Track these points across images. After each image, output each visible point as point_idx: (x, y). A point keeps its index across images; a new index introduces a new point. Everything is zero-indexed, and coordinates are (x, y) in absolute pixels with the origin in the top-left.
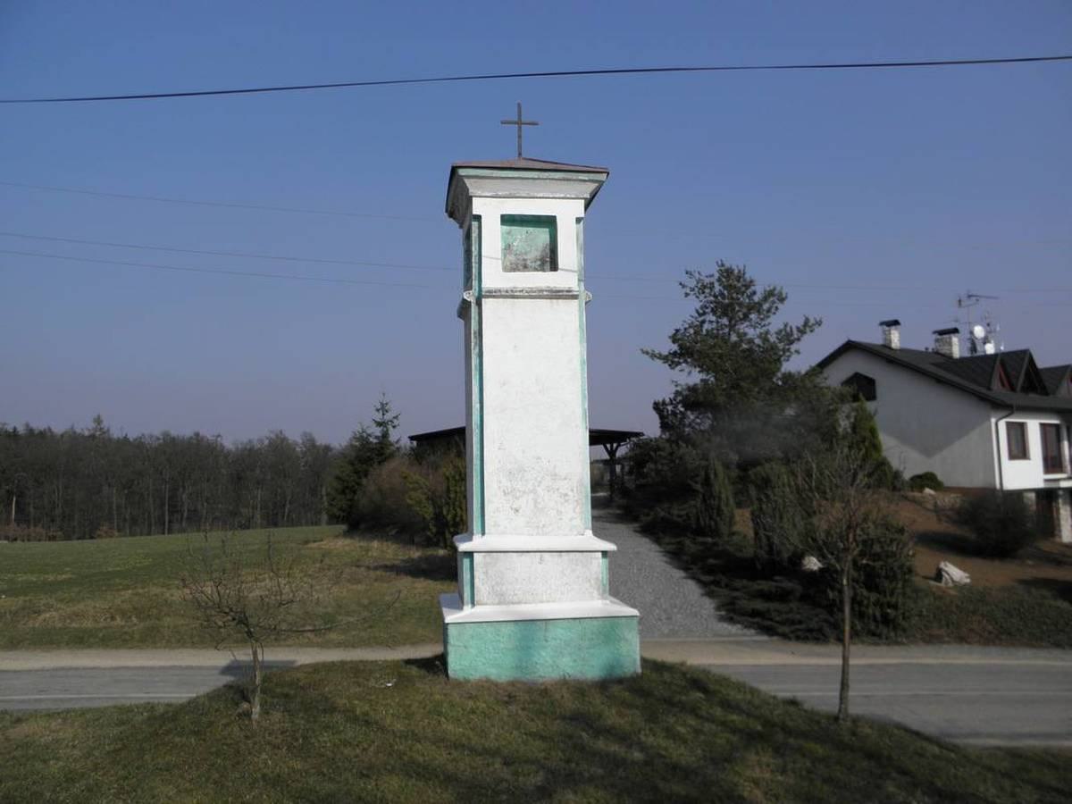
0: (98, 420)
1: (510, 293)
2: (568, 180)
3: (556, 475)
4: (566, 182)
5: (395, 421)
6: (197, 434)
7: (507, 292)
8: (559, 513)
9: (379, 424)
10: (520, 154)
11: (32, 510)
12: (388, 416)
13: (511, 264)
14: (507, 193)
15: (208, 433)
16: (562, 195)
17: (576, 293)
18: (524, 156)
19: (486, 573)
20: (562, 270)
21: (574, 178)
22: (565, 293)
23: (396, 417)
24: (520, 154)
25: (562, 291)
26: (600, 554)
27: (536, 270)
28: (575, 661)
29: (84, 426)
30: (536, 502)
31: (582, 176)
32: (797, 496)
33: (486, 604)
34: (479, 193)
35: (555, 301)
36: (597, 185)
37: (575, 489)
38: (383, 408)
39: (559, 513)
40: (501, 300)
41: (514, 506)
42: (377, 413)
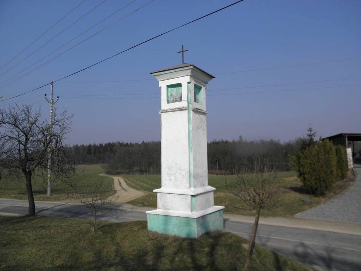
0: (241, 137)
1: (167, 111)
2: (182, 70)
3: (181, 169)
4: (182, 71)
5: (315, 134)
6: (272, 140)
7: (167, 110)
8: (182, 181)
9: (309, 136)
10: (183, 62)
11: (222, 165)
12: (312, 133)
13: (172, 100)
14: (167, 78)
15: (275, 139)
16: (182, 76)
17: (185, 108)
18: (184, 63)
19: (160, 199)
20: (183, 101)
21: (183, 69)
22: (182, 109)
23: (315, 133)
24: (183, 62)
25: (181, 108)
26: (190, 196)
27: (179, 101)
28: (178, 230)
29: (237, 139)
30: (176, 178)
31: (185, 68)
32: (38, 193)
33: (160, 209)
34: (160, 80)
35: (181, 111)
36: (191, 70)
37: (186, 174)
38: (310, 130)
39: (182, 181)
40: (166, 113)
41: (170, 179)
42: (308, 132)
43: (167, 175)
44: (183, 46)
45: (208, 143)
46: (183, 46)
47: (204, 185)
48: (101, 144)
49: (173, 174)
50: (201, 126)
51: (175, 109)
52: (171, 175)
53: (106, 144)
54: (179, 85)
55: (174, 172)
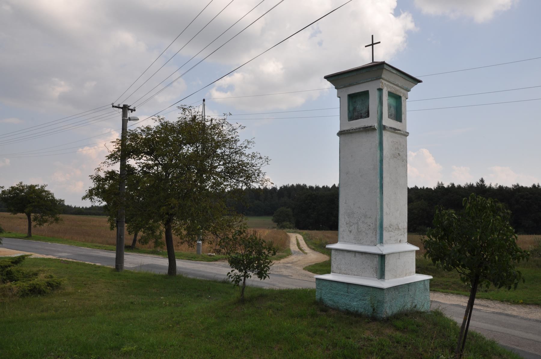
27: (365, 117)
30: (358, 229)
43: (347, 224)
47: (400, 241)
51: (360, 128)
53: (281, 188)
54: (366, 94)
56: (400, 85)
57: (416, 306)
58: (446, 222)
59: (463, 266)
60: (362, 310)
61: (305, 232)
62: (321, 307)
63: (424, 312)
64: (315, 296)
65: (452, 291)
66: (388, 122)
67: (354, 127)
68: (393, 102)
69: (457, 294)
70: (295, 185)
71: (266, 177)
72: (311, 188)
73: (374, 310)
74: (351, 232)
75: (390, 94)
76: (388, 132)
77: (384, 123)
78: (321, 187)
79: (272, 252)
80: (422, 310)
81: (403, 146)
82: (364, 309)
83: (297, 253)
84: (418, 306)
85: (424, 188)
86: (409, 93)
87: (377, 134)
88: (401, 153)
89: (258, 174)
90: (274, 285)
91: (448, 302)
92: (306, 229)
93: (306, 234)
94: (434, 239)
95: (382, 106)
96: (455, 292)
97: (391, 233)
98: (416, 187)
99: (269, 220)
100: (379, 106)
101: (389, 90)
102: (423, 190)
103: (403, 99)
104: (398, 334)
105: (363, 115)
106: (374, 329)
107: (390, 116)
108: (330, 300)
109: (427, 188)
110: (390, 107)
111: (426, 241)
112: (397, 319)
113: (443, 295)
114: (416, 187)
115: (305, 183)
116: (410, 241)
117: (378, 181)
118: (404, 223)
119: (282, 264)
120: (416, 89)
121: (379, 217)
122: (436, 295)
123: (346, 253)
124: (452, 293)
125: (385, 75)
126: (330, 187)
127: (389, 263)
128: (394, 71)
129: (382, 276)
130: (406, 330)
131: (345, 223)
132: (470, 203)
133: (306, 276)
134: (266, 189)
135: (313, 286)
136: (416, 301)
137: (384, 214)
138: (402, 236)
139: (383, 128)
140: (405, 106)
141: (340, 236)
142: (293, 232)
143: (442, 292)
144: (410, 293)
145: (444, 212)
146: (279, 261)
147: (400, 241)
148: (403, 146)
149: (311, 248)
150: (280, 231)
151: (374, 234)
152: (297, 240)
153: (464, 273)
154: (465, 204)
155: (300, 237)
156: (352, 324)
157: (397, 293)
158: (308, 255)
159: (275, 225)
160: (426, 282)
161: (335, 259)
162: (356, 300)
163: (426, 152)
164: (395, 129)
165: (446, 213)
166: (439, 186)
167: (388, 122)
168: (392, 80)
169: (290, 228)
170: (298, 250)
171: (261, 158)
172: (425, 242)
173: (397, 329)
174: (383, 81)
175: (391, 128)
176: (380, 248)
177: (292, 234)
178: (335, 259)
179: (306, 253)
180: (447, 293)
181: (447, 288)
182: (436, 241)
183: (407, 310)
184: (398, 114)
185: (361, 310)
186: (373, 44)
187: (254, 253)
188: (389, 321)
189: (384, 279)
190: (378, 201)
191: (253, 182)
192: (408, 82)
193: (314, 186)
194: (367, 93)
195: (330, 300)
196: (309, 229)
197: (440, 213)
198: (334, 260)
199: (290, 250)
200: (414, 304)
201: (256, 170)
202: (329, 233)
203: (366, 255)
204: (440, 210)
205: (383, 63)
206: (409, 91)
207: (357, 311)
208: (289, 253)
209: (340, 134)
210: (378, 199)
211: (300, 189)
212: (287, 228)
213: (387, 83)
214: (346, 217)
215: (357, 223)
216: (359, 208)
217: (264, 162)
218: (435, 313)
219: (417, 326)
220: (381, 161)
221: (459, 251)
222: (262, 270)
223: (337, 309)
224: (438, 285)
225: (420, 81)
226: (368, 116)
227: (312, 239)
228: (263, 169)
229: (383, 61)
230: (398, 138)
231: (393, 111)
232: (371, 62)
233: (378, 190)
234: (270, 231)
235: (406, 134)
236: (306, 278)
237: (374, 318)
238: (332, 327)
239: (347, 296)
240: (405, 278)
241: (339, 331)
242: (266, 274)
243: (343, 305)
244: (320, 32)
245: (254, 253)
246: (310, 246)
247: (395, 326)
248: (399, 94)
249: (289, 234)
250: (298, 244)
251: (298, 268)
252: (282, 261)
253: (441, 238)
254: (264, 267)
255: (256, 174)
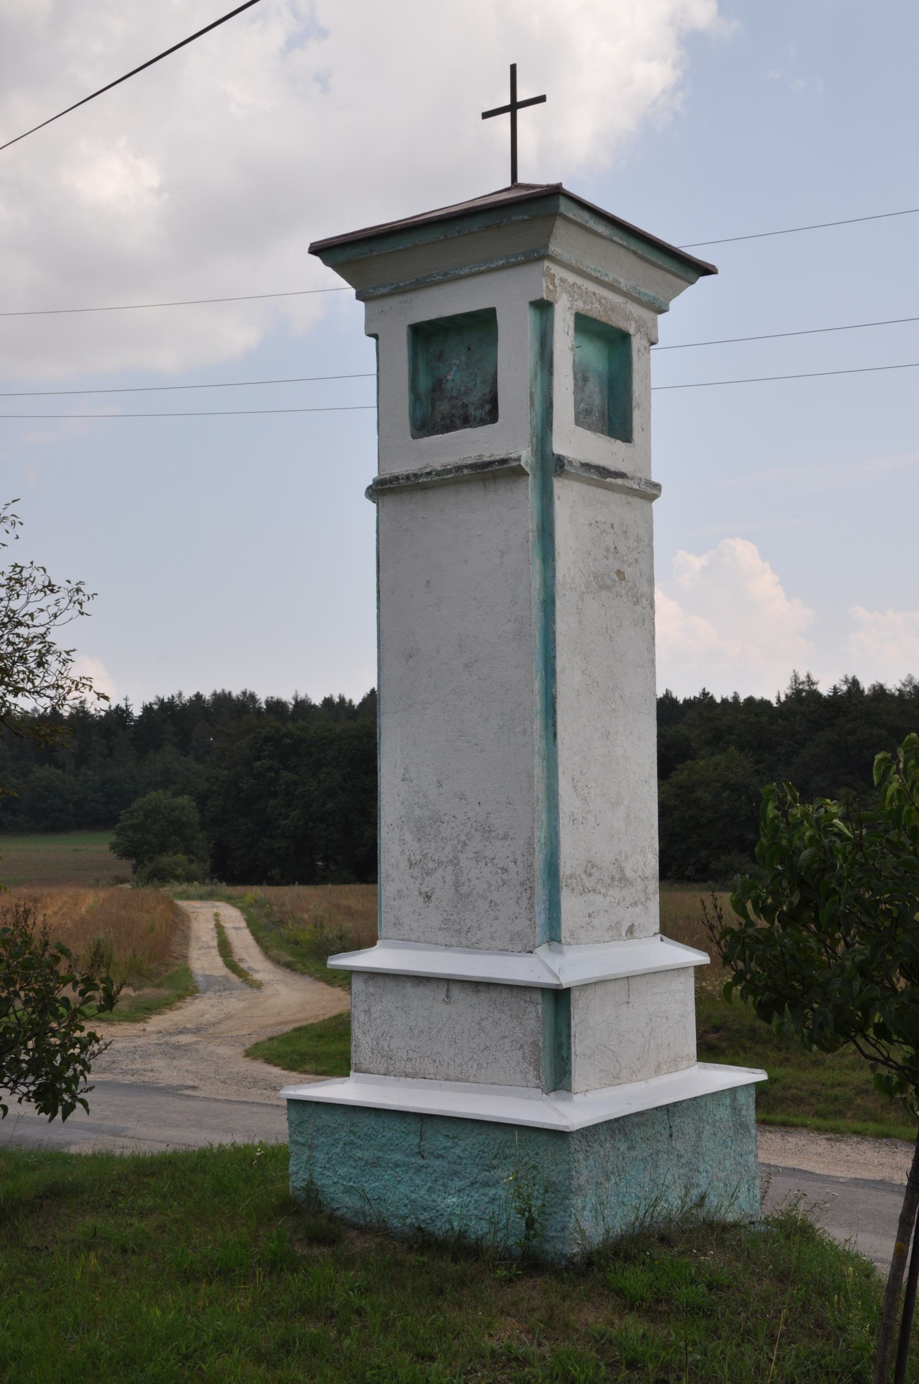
27: (483, 422)
30: (457, 884)
41: (424, 889)
43: (412, 865)
44: (513, 68)
45: (574, 361)
46: (513, 68)
47: (631, 931)
48: (123, 706)
49: (440, 863)
50: (619, 572)
51: (459, 468)
52: (431, 865)
53: (147, 709)
54: (485, 321)
55: (448, 849)
56: (624, 284)
57: (703, 1198)
58: (806, 853)
59: (882, 1031)
60: (484, 1227)
61: (255, 892)
62: (315, 1223)
63: (735, 1225)
64: (286, 1178)
65: (859, 1126)
66: (573, 441)
67: (437, 464)
68: (595, 356)
69: (879, 1136)
70: (207, 695)
71: (75, 672)
72: (276, 706)
73: (530, 1223)
74: (428, 897)
75: (585, 325)
76: (576, 486)
77: (560, 446)
78: (317, 701)
79: (99, 994)
80: (731, 1218)
81: (638, 539)
82: (491, 1222)
83: (223, 986)
84: (713, 1200)
85: (736, 698)
86: (660, 317)
87: (527, 494)
88: (628, 571)
89: (42, 655)
90: (116, 1133)
91: (842, 1172)
92: (258, 882)
93: (258, 904)
94: (762, 923)
95: (551, 373)
96: (872, 1126)
97: (592, 896)
98: (705, 694)
99: (97, 847)
100: (538, 373)
101: (580, 306)
102: (731, 706)
103: (637, 343)
104: (634, 1326)
105: (471, 410)
106: (531, 1311)
107: (582, 418)
108: (348, 1191)
109: (750, 700)
110: (585, 379)
111: (728, 931)
112: (627, 1258)
113: (821, 1144)
114: (705, 694)
115: (250, 689)
116: (672, 928)
117: (537, 685)
118: (645, 855)
119: (154, 1039)
120: (690, 302)
121: (541, 835)
122: (795, 1140)
123: (409, 989)
124: (857, 1133)
125: (564, 242)
126: (357, 701)
127: (588, 1025)
128: (602, 228)
129: (559, 1078)
130: (663, 1307)
131: (404, 864)
132: (905, 772)
133: (255, 1083)
134: (81, 714)
135: (274, 1129)
136: (702, 1180)
137: (563, 821)
138: (638, 909)
139: (553, 466)
140: (647, 375)
141: (386, 918)
142: (201, 898)
143: (819, 1130)
144: (678, 1145)
145: (797, 811)
146: (140, 1026)
147: (631, 931)
148: (638, 539)
149: (277, 962)
150: (148, 891)
151: (524, 902)
152: (220, 928)
153: (887, 1061)
154: (885, 776)
155: (232, 917)
156: (441, 1291)
157: (623, 1147)
158: (267, 991)
159: (126, 866)
160: (742, 1098)
161: (368, 1012)
162: (457, 1183)
163: (745, 552)
164: (603, 472)
165: (805, 815)
166: (798, 692)
167: (573, 441)
168: (590, 265)
169: (190, 878)
170: (225, 971)
171: (50, 588)
172: (723, 936)
173: (630, 1304)
174: (555, 270)
175: (587, 466)
176: (549, 961)
177: (197, 904)
178: (368, 1012)
179: (257, 986)
180: (836, 1133)
181: (839, 1114)
182: (770, 932)
183: (669, 1220)
184: (615, 409)
185: (478, 1228)
186: (514, 107)
187: (18, 1004)
188: (596, 1268)
189: (569, 1090)
190: (538, 771)
191: (17, 691)
192: (657, 274)
193: (288, 697)
194: (487, 313)
195: (348, 1191)
196: (271, 882)
197: (785, 814)
198: (362, 1018)
199: (187, 972)
200: (695, 1193)
201: (29, 642)
202: (349, 895)
203: (494, 994)
204: (782, 805)
205: (555, 192)
206: (661, 311)
207: (462, 1234)
208: (185, 987)
209: (380, 490)
210: (537, 760)
211: (230, 711)
212: (177, 878)
213: (571, 278)
214: (408, 837)
215: (455, 862)
216: (462, 797)
217: (64, 604)
218: (780, 1224)
219: (710, 1287)
220: (549, 604)
221: (862, 970)
222: (58, 1075)
223: (379, 1230)
224: (798, 1101)
225: (706, 270)
226: (492, 416)
227: (282, 922)
228: (59, 638)
229: (553, 181)
230: (614, 507)
231: (596, 394)
232: (508, 184)
233: (538, 724)
234: (102, 894)
235: (650, 492)
236: (254, 1095)
237: (531, 1262)
238: (359, 1312)
239: (419, 1169)
240: (655, 1082)
241: (386, 1327)
242: (74, 1096)
243: (403, 1211)
244: (323, 33)
245: (18, 1004)
246: (274, 952)
247: (620, 1292)
248: (622, 324)
249: (183, 904)
250: (225, 948)
251: (221, 1050)
252: (156, 1023)
253: (791, 919)
254: (68, 1061)
255: (32, 658)
